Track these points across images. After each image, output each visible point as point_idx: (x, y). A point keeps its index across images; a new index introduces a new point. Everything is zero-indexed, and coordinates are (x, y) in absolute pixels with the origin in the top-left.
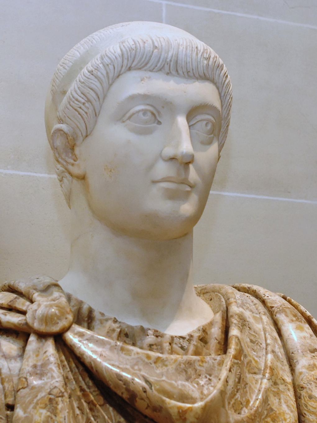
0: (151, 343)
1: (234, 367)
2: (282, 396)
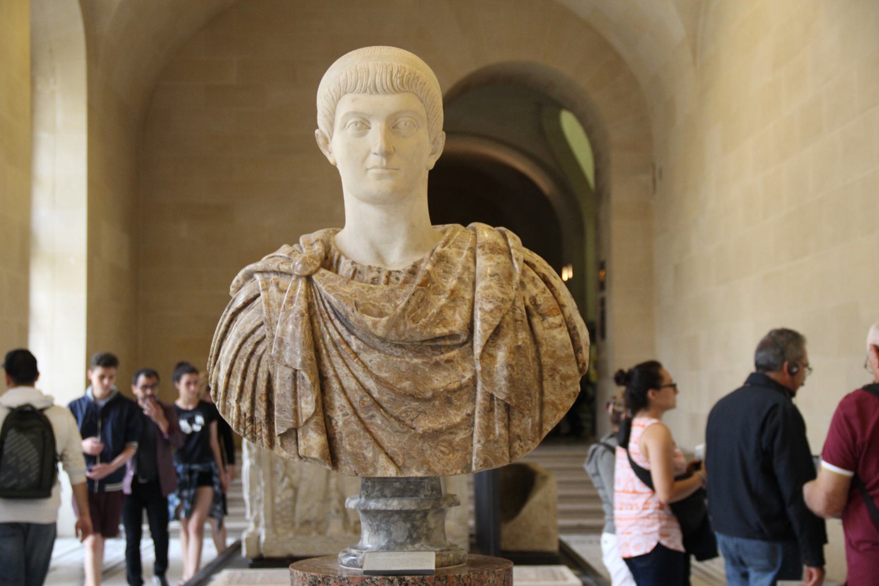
0: (374, 277)
2: (457, 309)
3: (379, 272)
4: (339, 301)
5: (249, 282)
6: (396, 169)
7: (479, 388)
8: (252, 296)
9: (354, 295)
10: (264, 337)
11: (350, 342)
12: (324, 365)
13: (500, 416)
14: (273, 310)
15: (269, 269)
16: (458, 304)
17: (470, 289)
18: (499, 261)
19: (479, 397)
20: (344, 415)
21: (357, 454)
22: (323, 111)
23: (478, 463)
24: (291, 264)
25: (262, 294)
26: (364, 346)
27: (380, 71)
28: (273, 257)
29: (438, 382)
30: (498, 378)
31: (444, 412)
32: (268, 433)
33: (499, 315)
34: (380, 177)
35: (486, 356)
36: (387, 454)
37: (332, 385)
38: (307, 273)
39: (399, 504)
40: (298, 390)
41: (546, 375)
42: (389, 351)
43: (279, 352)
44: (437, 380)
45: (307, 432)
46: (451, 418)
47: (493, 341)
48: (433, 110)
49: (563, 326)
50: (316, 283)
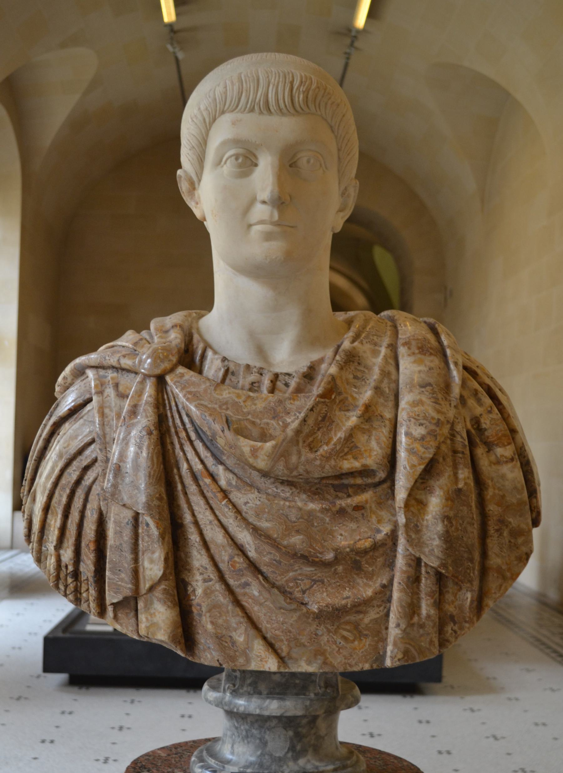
0: (253, 381)
1: (317, 406)
2: (374, 432)
3: (261, 374)
4: (201, 414)
5: (79, 381)
6: (292, 227)
7: (400, 549)
8: (80, 401)
9: (224, 407)
10: (95, 460)
11: (217, 475)
12: (179, 506)
13: (429, 590)
14: (109, 422)
15: (105, 363)
16: (374, 426)
17: (391, 404)
18: (432, 365)
19: (400, 562)
20: (205, 581)
21: (222, 637)
22: (188, 140)
23: (396, 656)
24: (136, 358)
25: (95, 398)
26: (236, 482)
27: (275, 80)
28: (113, 347)
29: (343, 538)
30: (429, 534)
31: (349, 581)
32: (98, 595)
33: (433, 444)
34: (268, 237)
35: (413, 502)
36: (265, 638)
37: (189, 537)
38: (158, 371)
39: (280, 707)
40: (140, 542)
41: (491, 531)
42: (272, 489)
43: (115, 486)
44: (341, 535)
45: (152, 603)
46: (359, 590)
47: (423, 481)
48: (346, 145)
49: (515, 460)
50: (171, 386)
